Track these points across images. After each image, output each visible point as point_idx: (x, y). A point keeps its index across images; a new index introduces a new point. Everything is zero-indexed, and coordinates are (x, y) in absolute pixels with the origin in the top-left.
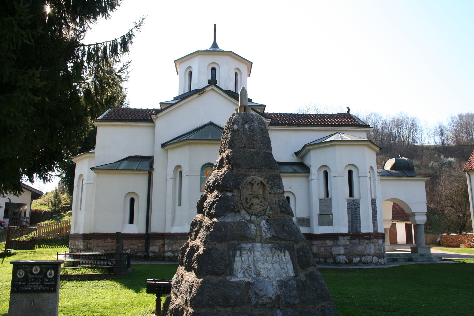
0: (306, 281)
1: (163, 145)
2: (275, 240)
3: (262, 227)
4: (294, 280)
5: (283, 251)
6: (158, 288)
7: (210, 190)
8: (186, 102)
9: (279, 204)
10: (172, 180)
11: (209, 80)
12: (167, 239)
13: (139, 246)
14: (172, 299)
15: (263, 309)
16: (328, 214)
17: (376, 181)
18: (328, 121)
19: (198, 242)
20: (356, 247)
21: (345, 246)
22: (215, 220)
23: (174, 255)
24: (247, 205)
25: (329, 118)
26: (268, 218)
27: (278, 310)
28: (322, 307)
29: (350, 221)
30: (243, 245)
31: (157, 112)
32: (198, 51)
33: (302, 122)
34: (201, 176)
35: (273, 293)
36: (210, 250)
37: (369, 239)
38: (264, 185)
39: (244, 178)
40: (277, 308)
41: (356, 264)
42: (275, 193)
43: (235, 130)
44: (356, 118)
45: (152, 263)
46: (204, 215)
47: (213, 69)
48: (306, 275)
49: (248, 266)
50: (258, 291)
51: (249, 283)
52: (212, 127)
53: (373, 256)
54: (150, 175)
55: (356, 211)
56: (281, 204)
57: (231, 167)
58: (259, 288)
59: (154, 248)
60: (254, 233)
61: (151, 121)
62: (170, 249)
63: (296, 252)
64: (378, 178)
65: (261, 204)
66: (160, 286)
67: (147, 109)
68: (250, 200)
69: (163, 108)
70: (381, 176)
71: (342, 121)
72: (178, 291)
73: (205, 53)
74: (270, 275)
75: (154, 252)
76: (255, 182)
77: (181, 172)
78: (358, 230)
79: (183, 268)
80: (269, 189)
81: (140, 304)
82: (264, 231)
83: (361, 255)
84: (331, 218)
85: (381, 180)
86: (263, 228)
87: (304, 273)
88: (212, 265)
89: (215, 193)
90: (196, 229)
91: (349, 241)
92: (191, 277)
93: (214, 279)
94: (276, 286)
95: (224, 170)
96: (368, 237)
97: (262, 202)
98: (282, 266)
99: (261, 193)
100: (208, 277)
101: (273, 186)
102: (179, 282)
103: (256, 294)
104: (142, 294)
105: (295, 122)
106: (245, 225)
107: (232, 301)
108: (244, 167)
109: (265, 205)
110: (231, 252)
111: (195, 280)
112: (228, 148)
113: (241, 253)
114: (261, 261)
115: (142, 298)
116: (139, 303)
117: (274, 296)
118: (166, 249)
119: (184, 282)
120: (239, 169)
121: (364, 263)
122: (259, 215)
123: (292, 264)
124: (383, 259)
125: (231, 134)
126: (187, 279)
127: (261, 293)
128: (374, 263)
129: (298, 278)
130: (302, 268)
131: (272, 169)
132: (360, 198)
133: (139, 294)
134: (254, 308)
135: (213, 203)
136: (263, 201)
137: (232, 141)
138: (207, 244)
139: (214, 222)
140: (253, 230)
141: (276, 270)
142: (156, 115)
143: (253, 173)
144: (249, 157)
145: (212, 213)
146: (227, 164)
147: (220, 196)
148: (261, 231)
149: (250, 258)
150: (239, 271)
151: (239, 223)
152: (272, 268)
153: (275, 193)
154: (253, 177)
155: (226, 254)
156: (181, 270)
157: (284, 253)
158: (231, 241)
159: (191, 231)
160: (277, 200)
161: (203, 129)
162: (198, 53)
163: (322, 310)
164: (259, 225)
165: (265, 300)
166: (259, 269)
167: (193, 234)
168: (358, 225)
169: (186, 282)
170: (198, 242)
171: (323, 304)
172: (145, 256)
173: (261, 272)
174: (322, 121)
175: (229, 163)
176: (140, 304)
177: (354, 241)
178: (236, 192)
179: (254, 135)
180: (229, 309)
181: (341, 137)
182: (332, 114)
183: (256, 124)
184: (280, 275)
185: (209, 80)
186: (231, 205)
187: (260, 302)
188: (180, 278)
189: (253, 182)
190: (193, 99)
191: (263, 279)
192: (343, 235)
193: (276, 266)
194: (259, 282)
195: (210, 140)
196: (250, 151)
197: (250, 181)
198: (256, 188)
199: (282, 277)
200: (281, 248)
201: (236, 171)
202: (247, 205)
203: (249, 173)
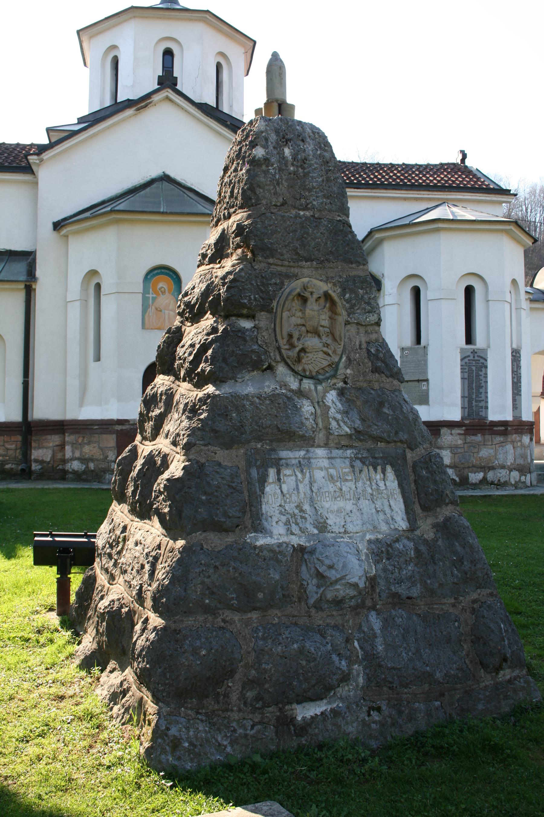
0: (435, 540)
1: (57, 226)
2: (361, 440)
3: (329, 408)
4: (408, 538)
5: (379, 468)
6: (60, 552)
7: (193, 314)
8: (108, 128)
9: (369, 352)
10: (78, 304)
11: (159, 76)
12: (71, 434)
13: (8, 449)
14: (99, 582)
15: (334, 613)
16: (418, 381)
17: (522, 311)
18: (420, 178)
19: (162, 444)
20: (476, 450)
21: (453, 448)
22: (210, 389)
23: (87, 467)
24: (290, 353)
25: (420, 172)
26: (341, 384)
27: (373, 613)
28: (474, 601)
29: (466, 395)
30: (284, 454)
31: (41, 149)
32: (132, 8)
33: (364, 179)
34: (144, 294)
35: (361, 573)
36: (202, 466)
37: (505, 433)
38: (333, 303)
39: (282, 283)
40: (370, 609)
41: (475, 486)
42: (358, 324)
43: (259, 160)
44: (479, 175)
45: (40, 485)
46: (177, 378)
47: (168, 54)
48: (435, 526)
49: (297, 507)
50: (324, 568)
51: (301, 550)
52: (165, 184)
53: (511, 471)
54: (29, 292)
55: (478, 375)
56: (373, 350)
57: (249, 255)
58: (327, 562)
59: (42, 453)
60: (310, 423)
61: (28, 169)
62: (77, 454)
63: (410, 470)
64: (525, 305)
65: (325, 349)
66: (65, 548)
67: (18, 145)
68: (299, 339)
69: (53, 140)
70: (531, 301)
71: (449, 179)
72: (115, 565)
73: (151, 12)
74: (350, 527)
75: (42, 462)
76: (312, 293)
77: (98, 286)
78: (483, 414)
79: (125, 508)
80: (344, 313)
81: (17, 588)
82: (335, 419)
83: (486, 468)
84: (425, 388)
85: (531, 309)
86: (332, 410)
87: (430, 521)
88: (208, 506)
89: (208, 321)
90: (157, 412)
91: (462, 437)
92: (149, 533)
93: (215, 541)
94: (367, 555)
95: (228, 264)
96: (503, 429)
97: (328, 345)
98: (379, 504)
99: (326, 323)
100: (198, 536)
101: (355, 305)
102: (118, 542)
103: (320, 576)
104: (21, 561)
105: (349, 178)
106: (287, 402)
107: (260, 595)
108: (282, 255)
109: (335, 352)
110: (254, 472)
111: (164, 543)
112: (240, 208)
113: (278, 473)
114: (329, 492)
115: (23, 572)
116: (16, 586)
117: (364, 579)
118: (68, 453)
119: (130, 544)
120: (271, 261)
121: (492, 483)
122: (321, 377)
123: (402, 500)
124: (528, 475)
125: (248, 171)
126: (138, 536)
127: (333, 575)
128: (512, 485)
129: (418, 533)
130: (425, 508)
131: (352, 263)
132: (489, 347)
133: (13, 561)
134: (313, 611)
135: (204, 347)
136: (329, 341)
137: (252, 189)
138: (193, 450)
139: (208, 396)
140: (307, 416)
141: (365, 516)
142: (38, 154)
143: (305, 271)
144: (295, 231)
145: (203, 371)
146: (238, 246)
147: (221, 328)
148: (328, 418)
149: (301, 486)
150: (275, 519)
151: (273, 397)
152: (354, 511)
153: (358, 324)
154: (306, 280)
155: (243, 477)
156: (119, 512)
157: (384, 472)
158: (253, 444)
159: (143, 418)
160: (363, 340)
161: (148, 190)
162: (133, 12)
163: (473, 609)
164: (321, 403)
165: (341, 591)
166: (325, 514)
167: (149, 426)
168: (482, 404)
169: (136, 544)
170: (162, 444)
171: (474, 596)
172: (23, 470)
173: (328, 521)
174: (406, 178)
175: (245, 243)
176: (17, 588)
177: (473, 438)
178: (263, 319)
179: (306, 175)
180: (254, 615)
181: (453, 213)
182: (428, 166)
183: (310, 147)
184: (375, 527)
185: (159, 76)
186: (253, 351)
187: (329, 596)
188: (118, 532)
189: (307, 295)
190: (123, 120)
191: (334, 538)
192: (451, 425)
193: (364, 504)
194: (325, 546)
195: (163, 213)
196: (297, 216)
197: (298, 290)
198: (313, 307)
199: (379, 532)
200: (374, 461)
201: (263, 265)
202: (290, 353)
203: (296, 270)
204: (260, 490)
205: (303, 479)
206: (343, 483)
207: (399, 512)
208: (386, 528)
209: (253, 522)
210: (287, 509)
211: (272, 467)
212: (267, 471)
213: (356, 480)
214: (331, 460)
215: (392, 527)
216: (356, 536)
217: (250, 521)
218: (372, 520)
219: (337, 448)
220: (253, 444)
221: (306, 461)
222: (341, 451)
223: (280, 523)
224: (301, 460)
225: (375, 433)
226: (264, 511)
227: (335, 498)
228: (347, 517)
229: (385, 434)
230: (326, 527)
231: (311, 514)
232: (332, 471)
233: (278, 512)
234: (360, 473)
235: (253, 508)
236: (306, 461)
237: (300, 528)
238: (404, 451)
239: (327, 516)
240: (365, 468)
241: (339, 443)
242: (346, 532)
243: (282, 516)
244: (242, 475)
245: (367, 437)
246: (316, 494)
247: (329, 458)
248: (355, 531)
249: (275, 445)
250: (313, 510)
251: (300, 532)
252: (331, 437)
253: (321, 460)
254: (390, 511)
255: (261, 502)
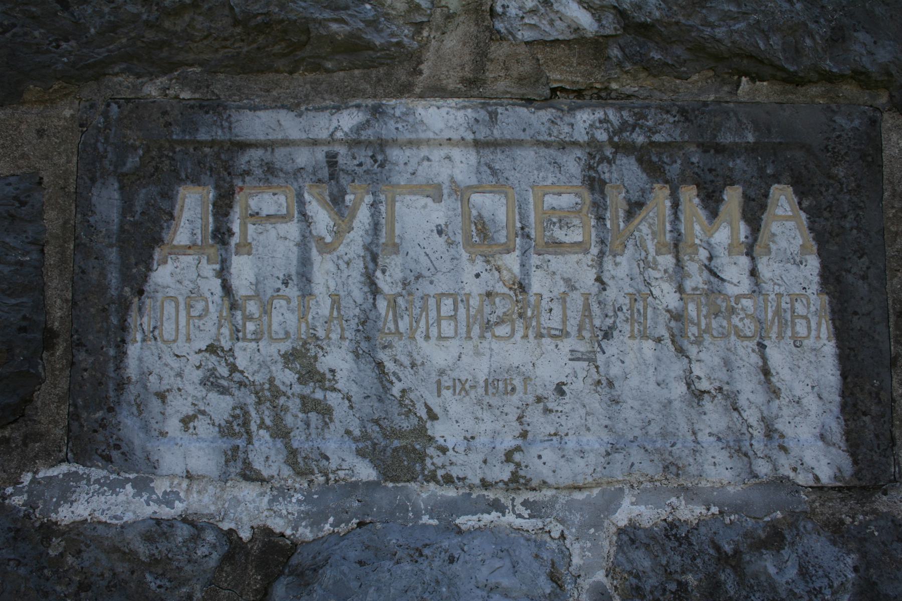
2: (651, 68)
4: (836, 531)
5: (733, 197)
30: (255, 124)
49: (289, 358)
74: (542, 462)
98: (706, 364)
110: (107, 202)
113: (223, 205)
114: (459, 298)
123: (829, 348)
141: (629, 414)
149: (323, 270)
150: (180, 406)
157: (754, 213)
173: (437, 430)
184: (672, 468)
191: (454, 507)
193: (636, 360)
199: (689, 493)
200: (711, 165)
204: (126, 278)
205: (338, 234)
206: (535, 260)
207: (811, 403)
208: (727, 476)
209: (74, 416)
210: (241, 363)
211: (196, 181)
212: (169, 196)
213: (606, 249)
214: (488, 155)
215: (763, 468)
216: (570, 505)
217: (65, 410)
218: (664, 435)
219: (528, 102)
220: (122, 82)
221: (364, 155)
222: (546, 115)
223: (201, 424)
224: (342, 150)
225: (720, 33)
226: (132, 368)
227: (488, 326)
228: (535, 416)
229: (776, 40)
230: (422, 457)
231: (354, 390)
232: (491, 205)
233: (198, 375)
234: (630, 215)
235: (81, 356)
236: (364, 155)
237: (293, 453)
238: (874, 123)
239: (435, 403)
240: (661, 197)
241: (537, 78)
242: (516, 482)
243: (213, 396)
244: (51, 214)
245: (679, 50)
246: (393, 304)
247: (478, 144)
248: (565, 475)
249: (221, 84)
250: (369, 374)
251: (287, 471)
252: (499, 51)
253: (437, 154)
254: (760, 398)
255: (123, 328)
